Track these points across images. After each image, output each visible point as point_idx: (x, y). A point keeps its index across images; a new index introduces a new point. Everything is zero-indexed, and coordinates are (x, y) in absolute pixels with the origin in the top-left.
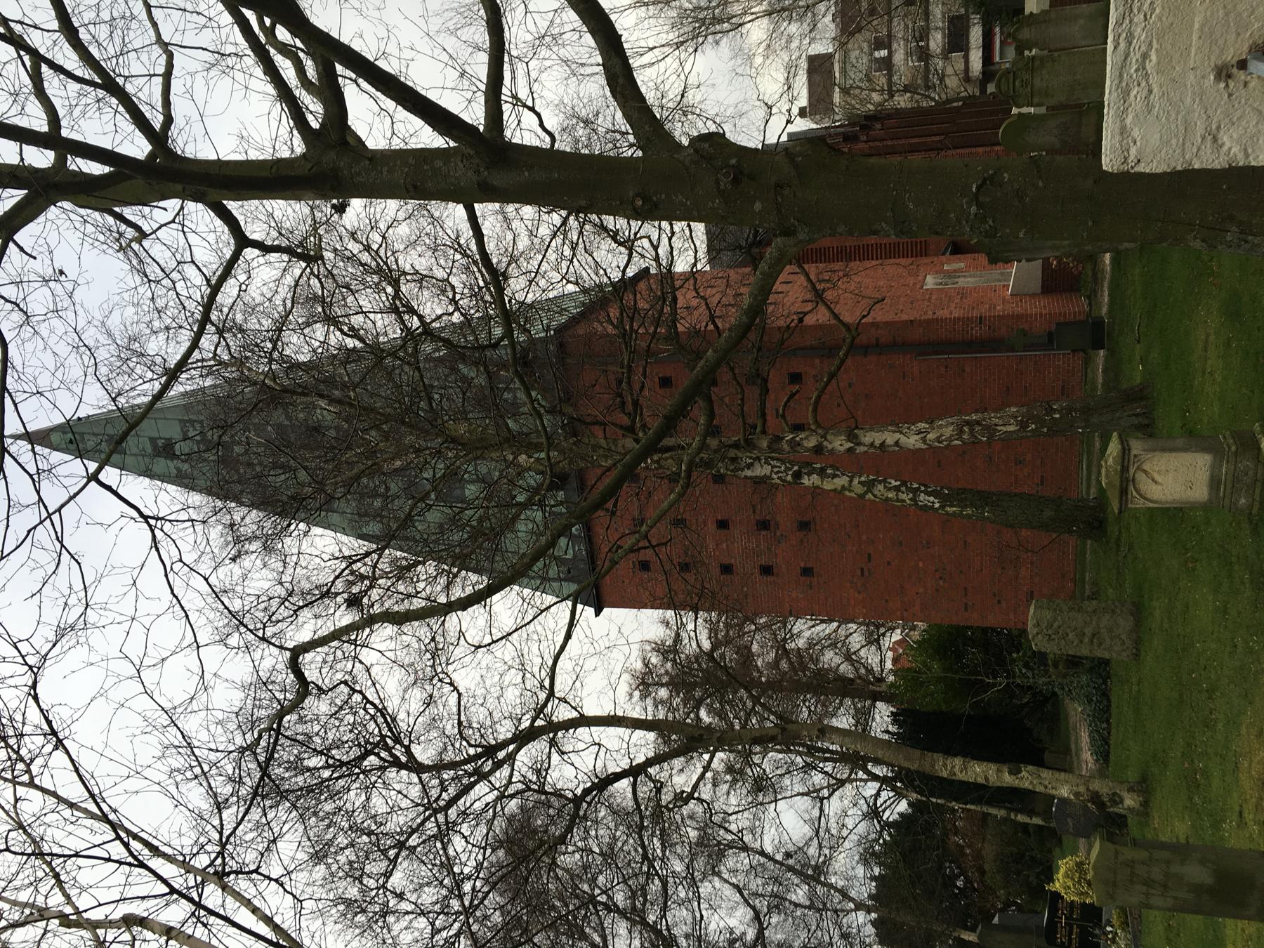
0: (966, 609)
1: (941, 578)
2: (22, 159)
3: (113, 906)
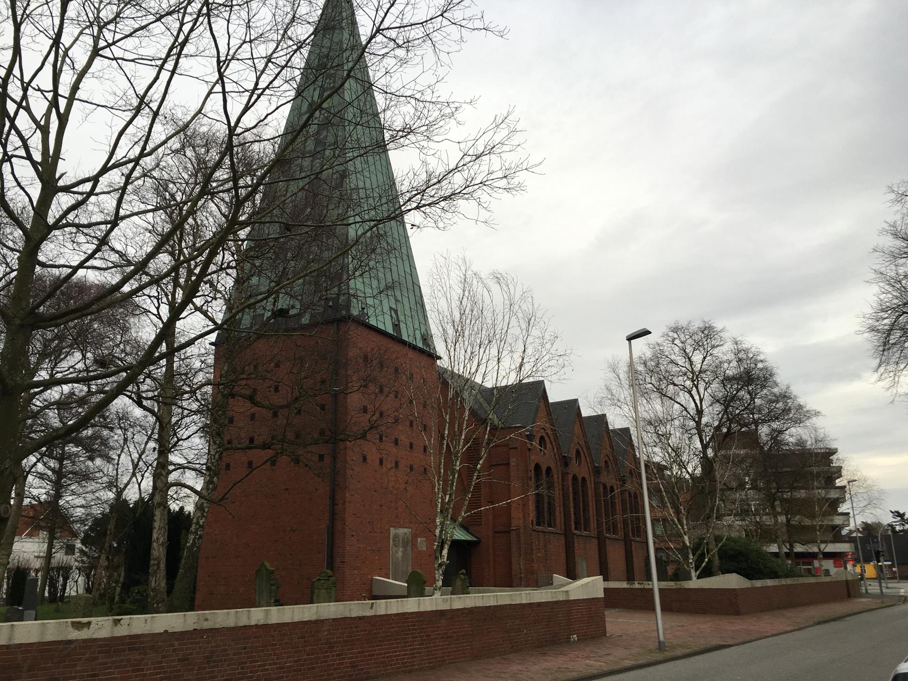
0: (206, 558)
2: (169, 71)
3: (391, 26)
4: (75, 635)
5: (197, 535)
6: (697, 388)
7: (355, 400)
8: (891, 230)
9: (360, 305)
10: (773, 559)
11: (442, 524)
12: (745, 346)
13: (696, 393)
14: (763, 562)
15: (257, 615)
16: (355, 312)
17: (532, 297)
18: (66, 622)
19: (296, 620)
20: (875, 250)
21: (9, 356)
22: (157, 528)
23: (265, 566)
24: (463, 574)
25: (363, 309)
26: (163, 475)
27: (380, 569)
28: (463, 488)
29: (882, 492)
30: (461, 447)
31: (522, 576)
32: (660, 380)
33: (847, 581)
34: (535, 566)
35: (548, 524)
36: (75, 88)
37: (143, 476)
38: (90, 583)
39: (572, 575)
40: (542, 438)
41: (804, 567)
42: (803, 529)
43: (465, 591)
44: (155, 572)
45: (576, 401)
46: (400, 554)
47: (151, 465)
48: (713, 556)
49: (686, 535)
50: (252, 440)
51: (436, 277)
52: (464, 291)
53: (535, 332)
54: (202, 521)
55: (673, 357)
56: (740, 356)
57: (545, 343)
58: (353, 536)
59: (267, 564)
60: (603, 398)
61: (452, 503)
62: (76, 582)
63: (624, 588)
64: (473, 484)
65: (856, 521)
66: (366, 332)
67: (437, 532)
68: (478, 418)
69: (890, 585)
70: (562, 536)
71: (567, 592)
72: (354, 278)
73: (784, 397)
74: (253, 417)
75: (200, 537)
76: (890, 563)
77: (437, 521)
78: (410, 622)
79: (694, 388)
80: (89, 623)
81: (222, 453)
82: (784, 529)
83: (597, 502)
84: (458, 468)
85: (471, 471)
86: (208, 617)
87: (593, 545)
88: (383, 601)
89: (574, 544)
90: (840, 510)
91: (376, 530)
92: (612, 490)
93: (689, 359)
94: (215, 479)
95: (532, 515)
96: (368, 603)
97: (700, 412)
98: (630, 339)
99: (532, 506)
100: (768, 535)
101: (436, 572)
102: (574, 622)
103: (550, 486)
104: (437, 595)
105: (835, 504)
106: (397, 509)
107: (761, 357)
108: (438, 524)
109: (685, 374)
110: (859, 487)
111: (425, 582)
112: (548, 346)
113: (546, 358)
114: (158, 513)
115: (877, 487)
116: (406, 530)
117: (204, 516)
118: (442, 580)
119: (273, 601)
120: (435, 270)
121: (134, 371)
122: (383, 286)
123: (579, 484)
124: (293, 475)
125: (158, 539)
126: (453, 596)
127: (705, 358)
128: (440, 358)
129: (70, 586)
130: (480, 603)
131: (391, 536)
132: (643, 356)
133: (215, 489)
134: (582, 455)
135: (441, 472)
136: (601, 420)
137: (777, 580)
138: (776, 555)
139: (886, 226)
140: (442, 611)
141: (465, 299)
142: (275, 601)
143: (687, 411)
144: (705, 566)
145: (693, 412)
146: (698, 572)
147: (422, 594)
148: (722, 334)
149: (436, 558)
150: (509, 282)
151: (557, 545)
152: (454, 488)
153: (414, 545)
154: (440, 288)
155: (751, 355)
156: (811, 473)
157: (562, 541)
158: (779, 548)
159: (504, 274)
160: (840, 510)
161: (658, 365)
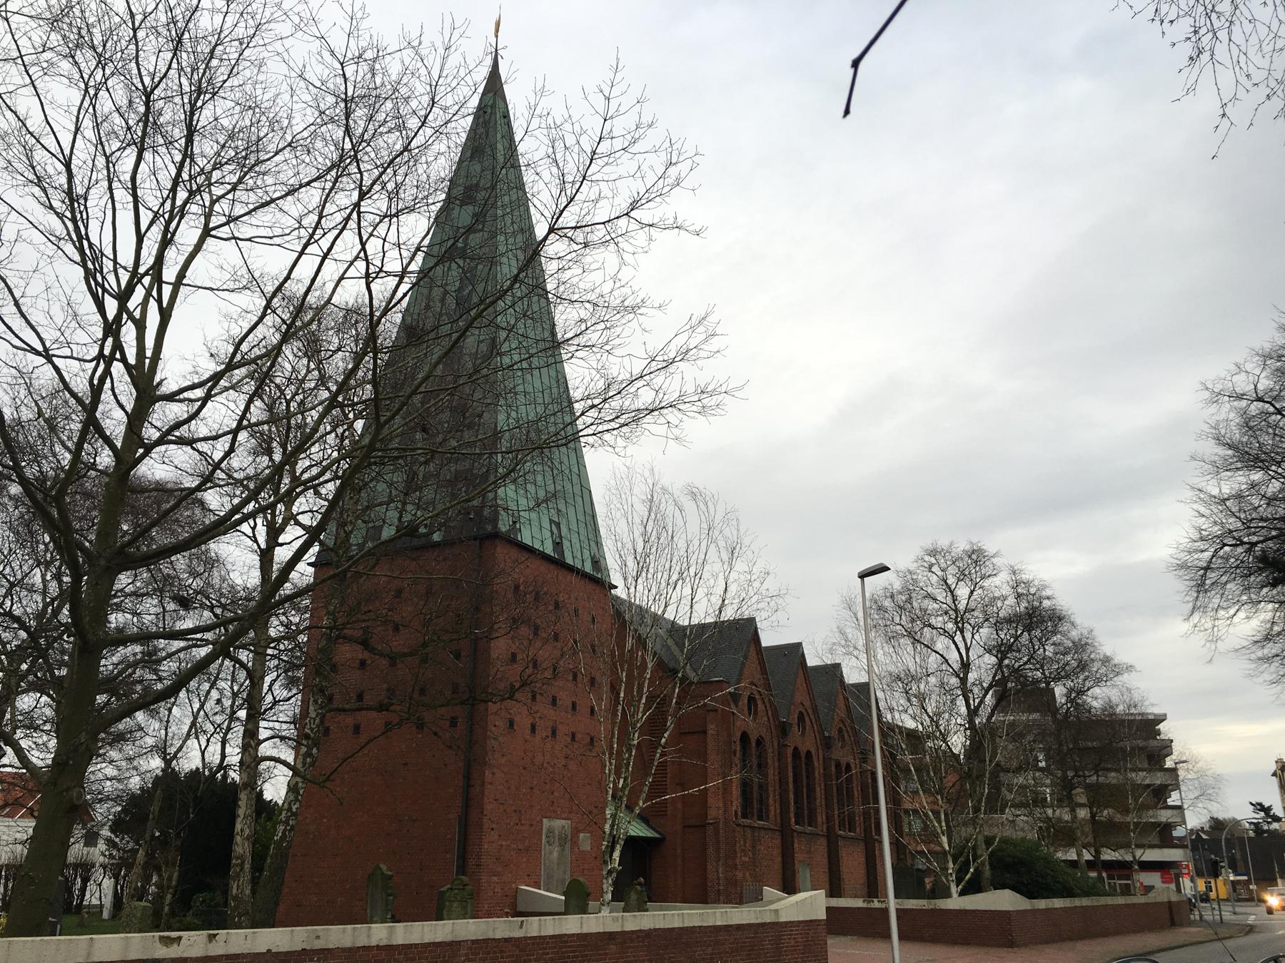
1: (315, 836)
4: (162, 952)
5: (289, 825)
6: (962, 632)
7: (500, 647)
8: (1212, 433)
9: (511, 519)
10: (1070, 870)
11: (614, 816)
12: (1024, 577)
13: (961, 639)
14: (1052, 873)
15: (379, 933)
16: (503, 527)
17: (738, 519)
18: (154, 936)
19: (426, 941)
20: (1193, 458)
21: (92, 605)
22: (242, 817)
23: (381, 869)
24: (640, 884)
25: (514, 523)
26: (251, 746)
27: (529, 875)
28: (643, 764)
29: (1218, 778)
30: (640, 715)
31: (721, 888)
32: (913, 621)
33: (1169, 902)
34: (739, 875)
35: (758, 816)
36: (181, 275)
37: (208, 741)
38: (119, 887)
39: (789, 887)
40: (751, 700)
41: (1119, 882)
42: (1112, 827)
43: (641, 908)
44: (238, 876)
45: (800, 645)
46: (555, 854)
47: (219, 726)
48: (983, 863)
49: (944, 835)
50: (360, 697)
51: (614, 491)
52: (650, 512)
53: (740, 566)
54: (296, 806)
55: (930, 590)
56: (1019, 590)
57: (752, 580)
58: (492, 829)
59: (383, 867)
60: (834, 644)
61: (628, 789)
62: (100, 885)
63: (858, 908)
64: (656, 763)
65: (1195, 819)
66: (514, 553)
67: (607, 828)
68: (666, 670)
69: (1238, 910)
70: (777, 833)
71: (776, 911)
72: (505, 485)
73: (1080, 646)
74: (363, 663)
75: (293, 828)
76: (1246, 878)
77: (607, 812)
78: (570, 947)
79: (958, 632)
80: (180, 938)
81: (324, 716)
82: (1087, 829)
83: (827, 789)
84: (636, 742)
85: (654, 746)
86: (321, 934)
87: (821, 847)
88: (537, 918)
89: (793, 846)
90: (1170, 802)
91: (523, 822)
92: (848, 768)
93: (952, 592)
94: (315, 751)
95: (736, 805)
96: (517, 921)
97: (966, 666)
98: (863, 576)
99: (736, 791)
100: (1065, 835)
101: (604, 881)
102: (785, 951)
103: (761, 766)
104: (605, 912)
105: (1160, 794)
106: (552, 793)
107: (1048, 592)
108: (609, 816)
109: (946, 613)
110: (1188, 770)
111: (589, 895)
112: (756, 584)
113: (755, 599)
114: (243, 796)
115: (1212, 771)
116: (563, 822)
117: (299, 800)
118: (612, 891)
119: (389, 916)
120: (613, 482)
121: (242, 625)
122: (542, 494)
123: (802, 760)
124: (414, 745)
125: (242, 830)
126: (625, 914)
127: (972, 592)
128: (616, 587)
129: (91, 892)
130: (661, 924)
131: (544, 832)
132: (890, 587)
133: (312, 764)
134: (807, 719)
135: (613, 748)
136: (833, 671)
137: (1068, 900)
138: (1073, 864)
139: (1206, 428)
140: (611, 933)
141: (651, 523)
142: (393, 917)
143: (949, 664)
144: (969, 879)
145: (956, 666)
146: (960, 887)
147: (583, 910)
148: (995, 560)
149: (605, 862)
150: (707, 498)
151: (770, 846)
152: (630, 769)
153: (575, 843)
154: (619, 505)
155: (1033, 590)
156: (1123, 750)
157: (777, 841)
158: (1078, 855)
159: (701, 488)
160: (1170, 802)
161: (909, 600)
